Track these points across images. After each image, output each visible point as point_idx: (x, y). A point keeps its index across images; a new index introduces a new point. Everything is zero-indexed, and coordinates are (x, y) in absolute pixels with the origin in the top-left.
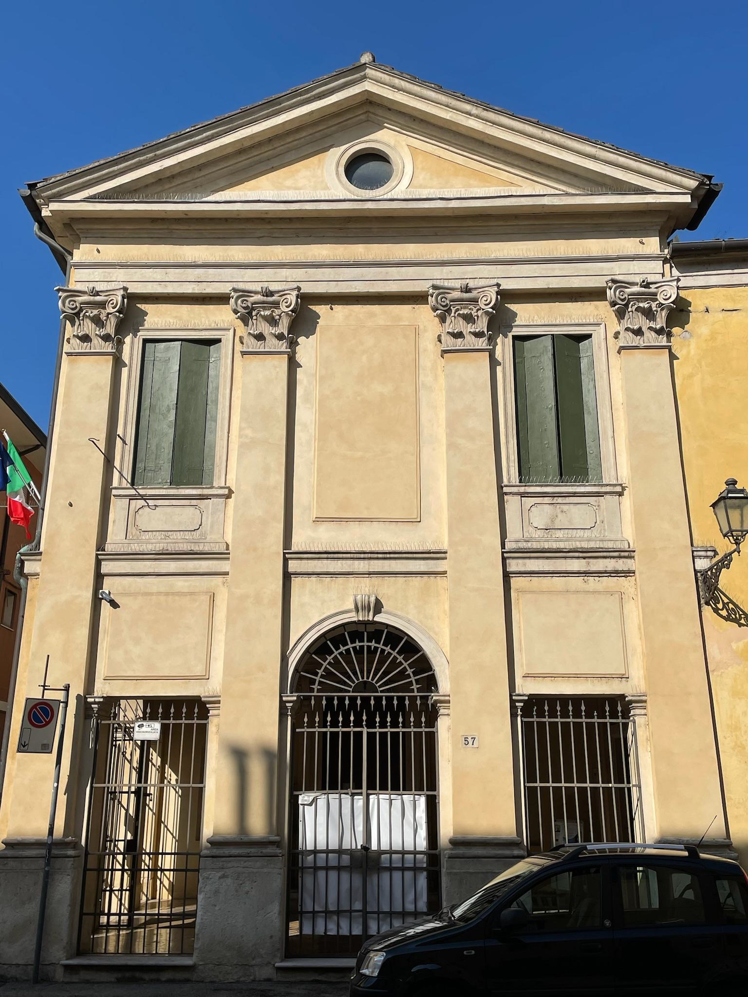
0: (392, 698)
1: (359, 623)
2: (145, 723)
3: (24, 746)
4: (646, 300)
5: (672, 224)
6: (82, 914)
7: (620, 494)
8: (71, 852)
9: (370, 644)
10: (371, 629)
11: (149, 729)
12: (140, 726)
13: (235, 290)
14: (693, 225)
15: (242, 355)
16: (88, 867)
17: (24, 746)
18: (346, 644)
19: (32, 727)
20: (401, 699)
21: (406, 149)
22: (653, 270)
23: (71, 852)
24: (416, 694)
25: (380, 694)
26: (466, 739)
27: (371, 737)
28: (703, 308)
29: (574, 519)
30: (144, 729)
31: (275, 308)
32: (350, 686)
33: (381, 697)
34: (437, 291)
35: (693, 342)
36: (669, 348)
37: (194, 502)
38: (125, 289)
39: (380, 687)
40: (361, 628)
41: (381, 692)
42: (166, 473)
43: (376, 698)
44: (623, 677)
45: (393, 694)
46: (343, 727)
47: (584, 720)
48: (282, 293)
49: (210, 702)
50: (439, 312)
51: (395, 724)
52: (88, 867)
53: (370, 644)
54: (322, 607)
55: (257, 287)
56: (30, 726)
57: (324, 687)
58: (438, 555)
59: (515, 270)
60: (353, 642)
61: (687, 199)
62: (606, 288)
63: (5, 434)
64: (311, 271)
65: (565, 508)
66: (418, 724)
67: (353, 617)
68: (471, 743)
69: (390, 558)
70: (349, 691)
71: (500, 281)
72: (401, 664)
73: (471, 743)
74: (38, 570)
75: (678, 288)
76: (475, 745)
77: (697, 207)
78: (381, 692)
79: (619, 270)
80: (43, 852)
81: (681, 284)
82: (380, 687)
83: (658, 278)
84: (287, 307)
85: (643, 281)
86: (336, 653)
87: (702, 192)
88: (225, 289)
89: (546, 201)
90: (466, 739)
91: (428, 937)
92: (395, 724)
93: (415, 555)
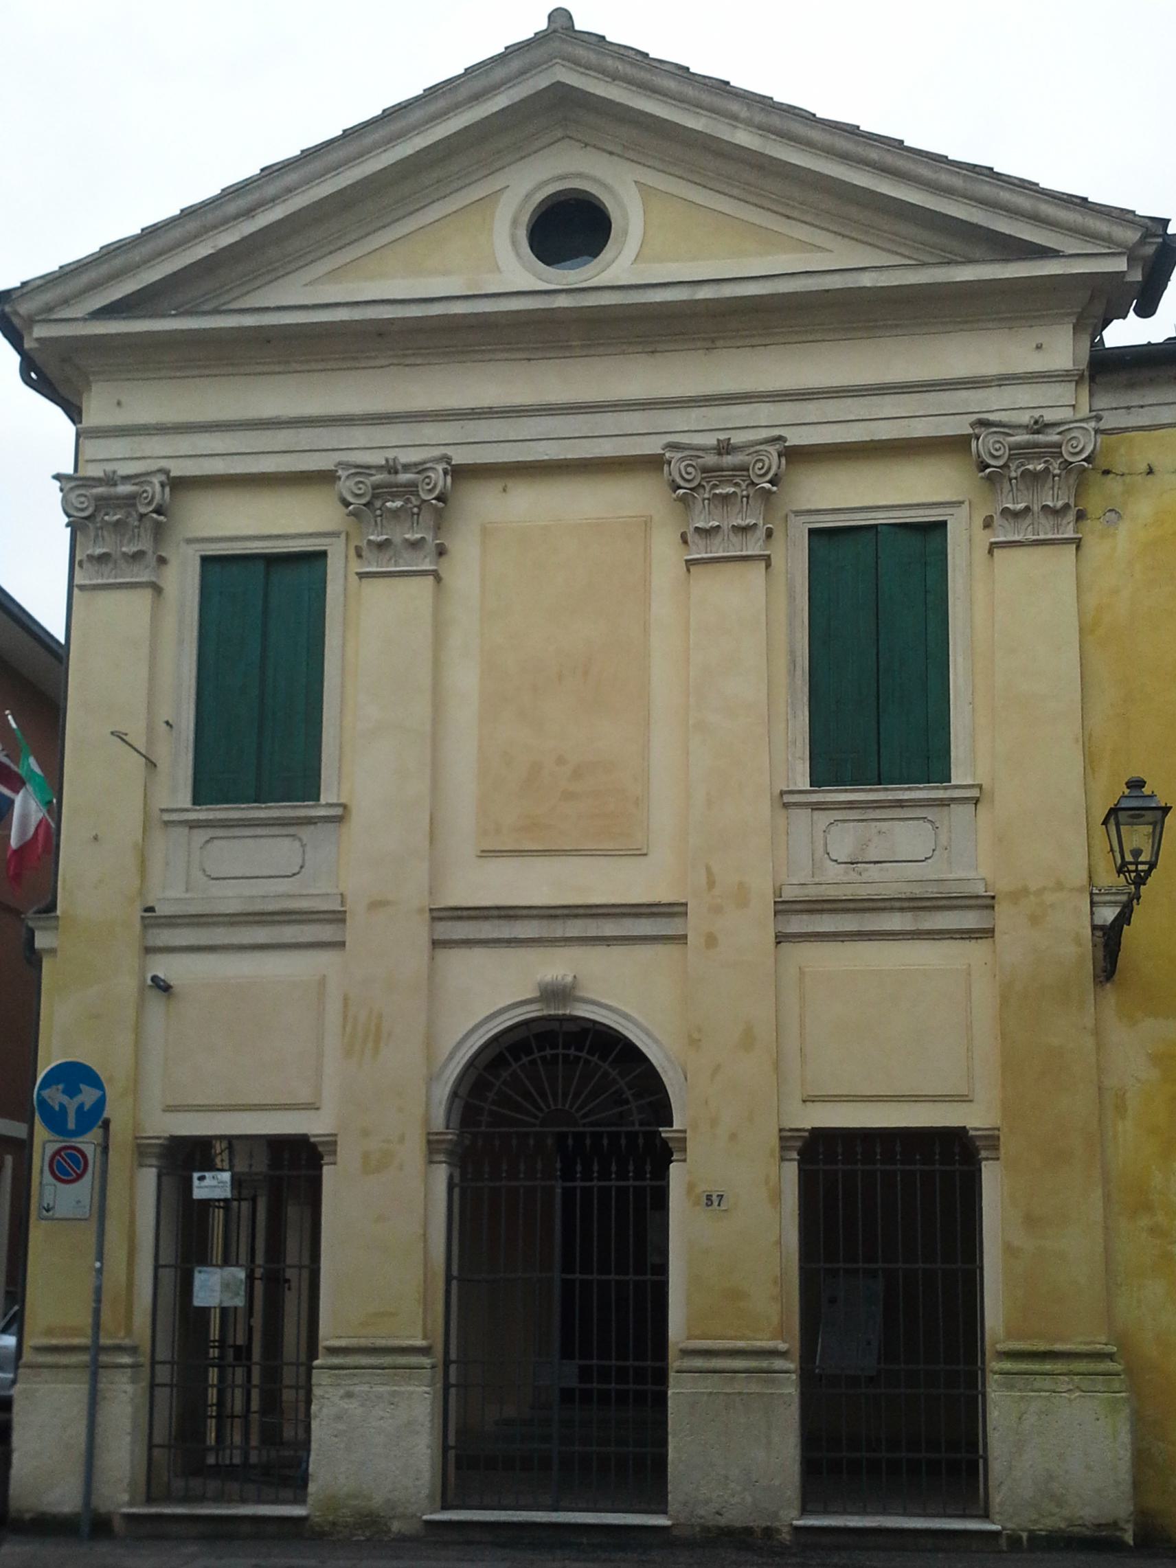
0: (600, 1135)
2: (207, 1174)
3: (48, 1211)
4: (1039, 456)
5: (1099, 309)
6: (151, 1446)
7: (977, 801)
8: (126, 1360)
12: (201, 1178)
13: (347, 466)
14: (1147, 309)
15: (360, 578)
16: (158, 1381)
17: (48, 1211)
18: (580, 1049)
19: (58, 1184)
21: (634, 189)
22: (1059, 404)
23: (126, 1360)
24: (637, 1128)
25: (581, 1129)
26: (709, 1198)
27: (568, 1194)
28: (1143, 467)
29: (899, 844)
30: (206, 1182)
31: (412, 493)
32: (536, 1117)
33: (583, 1134)
34: (680, 455)
35: (1123, 529)
36: (436, 575)
37: (292, 830)
38: (446, 459)
43: (628, 1134)
44: (964, 1099)
45: (619, 1129)
46: (617, 1179)
48: (420, 468)
49: (323, 1143)
50: (681, 491)
51: (622, 1176)
52: (158, 1381)
54: (493, 992)
55: (377, 458)
56: (55, 1182)
58: (675, 910)
59: (811, 411)
60: (541, 1049)
61: (1121, 265)
62: (969, 435)
63: (14, 725)
65: (884, 826)
66: (639, 1176)
67: (532, 1012)
68: (716, 1203)
69: (280, 922)
71: (449, 451)
73: (716, 1203)
74: (54, 945)
75: (1097, 431)
76: (723, 1208)
77: (1140, 278)
78: (584, 1125)
79: (994, 403)
81: (1103, 425)
83: (1067, 414)
84: (430, 491)
85: (1036, 422)
87: (1150, 250)
88: (652, 447)
89: (866, 280)
90: (709, 1198)
92: (604, 1175)
93: (955, 902)
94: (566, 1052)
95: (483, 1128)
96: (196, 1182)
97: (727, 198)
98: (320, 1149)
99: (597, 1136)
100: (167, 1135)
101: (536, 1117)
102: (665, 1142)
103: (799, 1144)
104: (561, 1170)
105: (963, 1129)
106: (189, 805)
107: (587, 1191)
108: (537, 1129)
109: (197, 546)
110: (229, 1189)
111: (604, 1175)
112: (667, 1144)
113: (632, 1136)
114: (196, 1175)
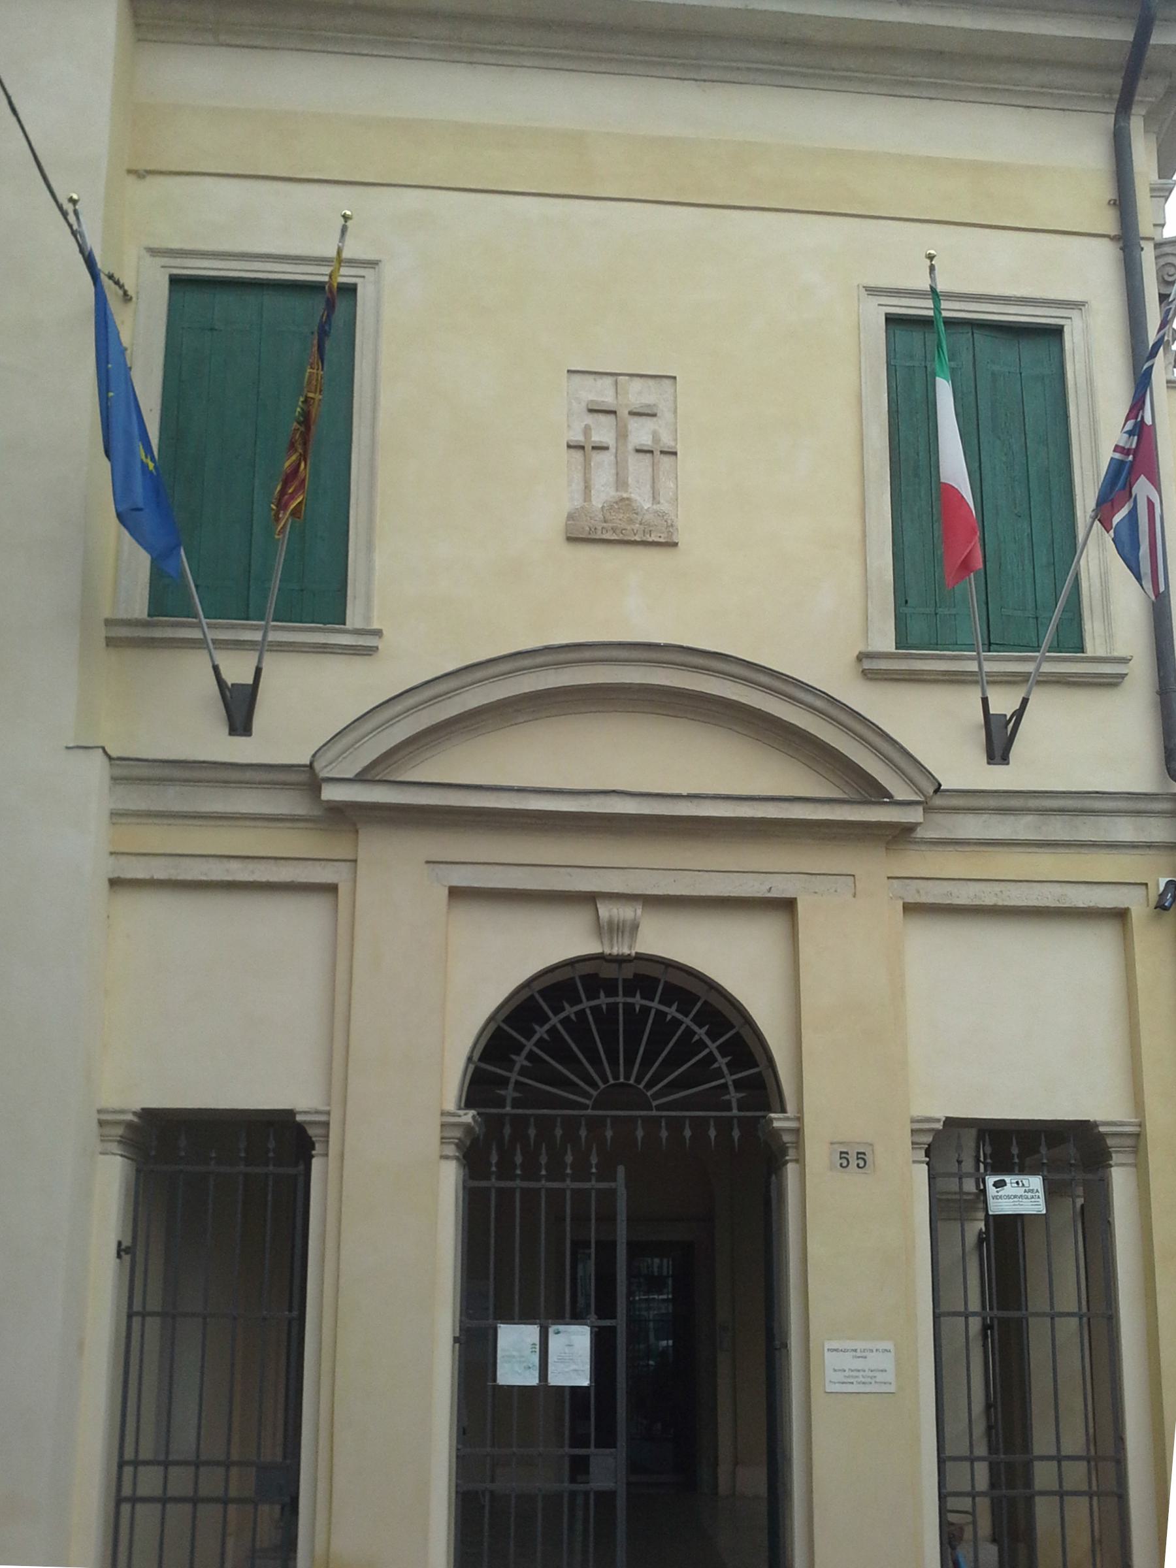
1: (600, 957)
2: (1007, 1179)
9: (695, 1028)
10: (628, 972)
11: (1020, 1191)
12: (1000, 1184)
20: (700, 1125)
25: (654, 1113)
30: (1009, 1190)
32: (586, 1095)
39: (656, 1096)
40: (609, 971)
41: (658, 1108)
42: (109, 635)
47: (493, 1182)
53: (695, 1028)
57: (528, 1098)
60: (557, 1010)
64: (989, 900)
66: (531, 1172)
70: (586, 1107)
72: (702, 1045)
78: (658, 1108)
80: (136, 1321)
82: (656, 1096)
86: (729, 1079)
91: (993, 1354)
94: (562, 1015)
95: (508, 1109)
96: (991, 1190)
97: (247, 50)
98: (311, 1131)
99: (676, 1125)
100: (137, 1107)
101: (586, 1095)
102: (777, 1133)
103: (120, 1131)
104: (497, 1165)
105: (291, 1113)
106: (893, 650)
107: (556, 1197)
108: (589, 1112)
109: (884, 300)
110: (1042, 1201)
111: (506, 1170)
112: (305, 1131)
113: (724, 1125)
114: (991, 1180)
